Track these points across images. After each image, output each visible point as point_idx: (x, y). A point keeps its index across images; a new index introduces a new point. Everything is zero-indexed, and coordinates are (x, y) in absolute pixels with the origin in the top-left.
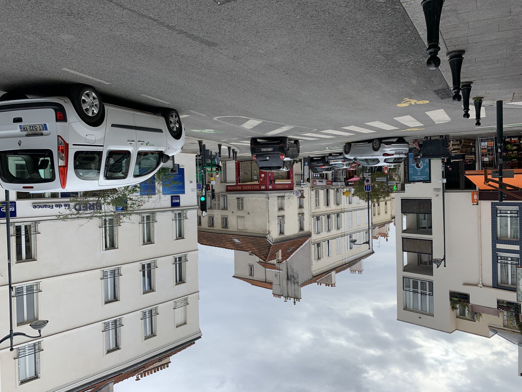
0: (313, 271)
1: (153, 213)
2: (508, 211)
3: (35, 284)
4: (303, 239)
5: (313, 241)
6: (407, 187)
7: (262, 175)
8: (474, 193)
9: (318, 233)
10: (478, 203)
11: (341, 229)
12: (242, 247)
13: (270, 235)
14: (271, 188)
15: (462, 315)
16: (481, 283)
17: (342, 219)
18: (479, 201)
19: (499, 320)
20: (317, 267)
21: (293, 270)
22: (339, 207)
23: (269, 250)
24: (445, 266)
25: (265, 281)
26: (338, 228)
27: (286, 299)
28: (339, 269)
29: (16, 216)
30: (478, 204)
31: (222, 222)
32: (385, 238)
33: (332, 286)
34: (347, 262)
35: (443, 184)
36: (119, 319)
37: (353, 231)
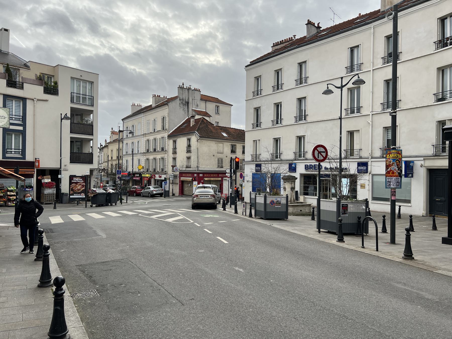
0: (167, 108)
2: (14, 153)
3: (349, 115)
4: (174, 134)
5: (167, 132)
6: (88, 173)
8: (38, 167)
9: (163, 138)
10: (35, 159)
11: (146, 140)
12: (221, 129)
13: (197, 138)
14: (195, 175)
15: (50, 77)
16: (35, 102)
17: (145, 148)
18: (34, 161)
20: (164, 112)
21: (183, 109)
22: (147, 157)
23: (199, 127)
24: (61, 114)
25: (207, 102)
26: (148, 140)
27: (190, 87)
28: (149, 109)
29: (358, 163)
30: (35, 158)
31: (236, 149)
32: (114, 130)
33: (155, 95)
34: (143, 114)
35: (61, 174)
36: (298, 85)
37: (137, 138)
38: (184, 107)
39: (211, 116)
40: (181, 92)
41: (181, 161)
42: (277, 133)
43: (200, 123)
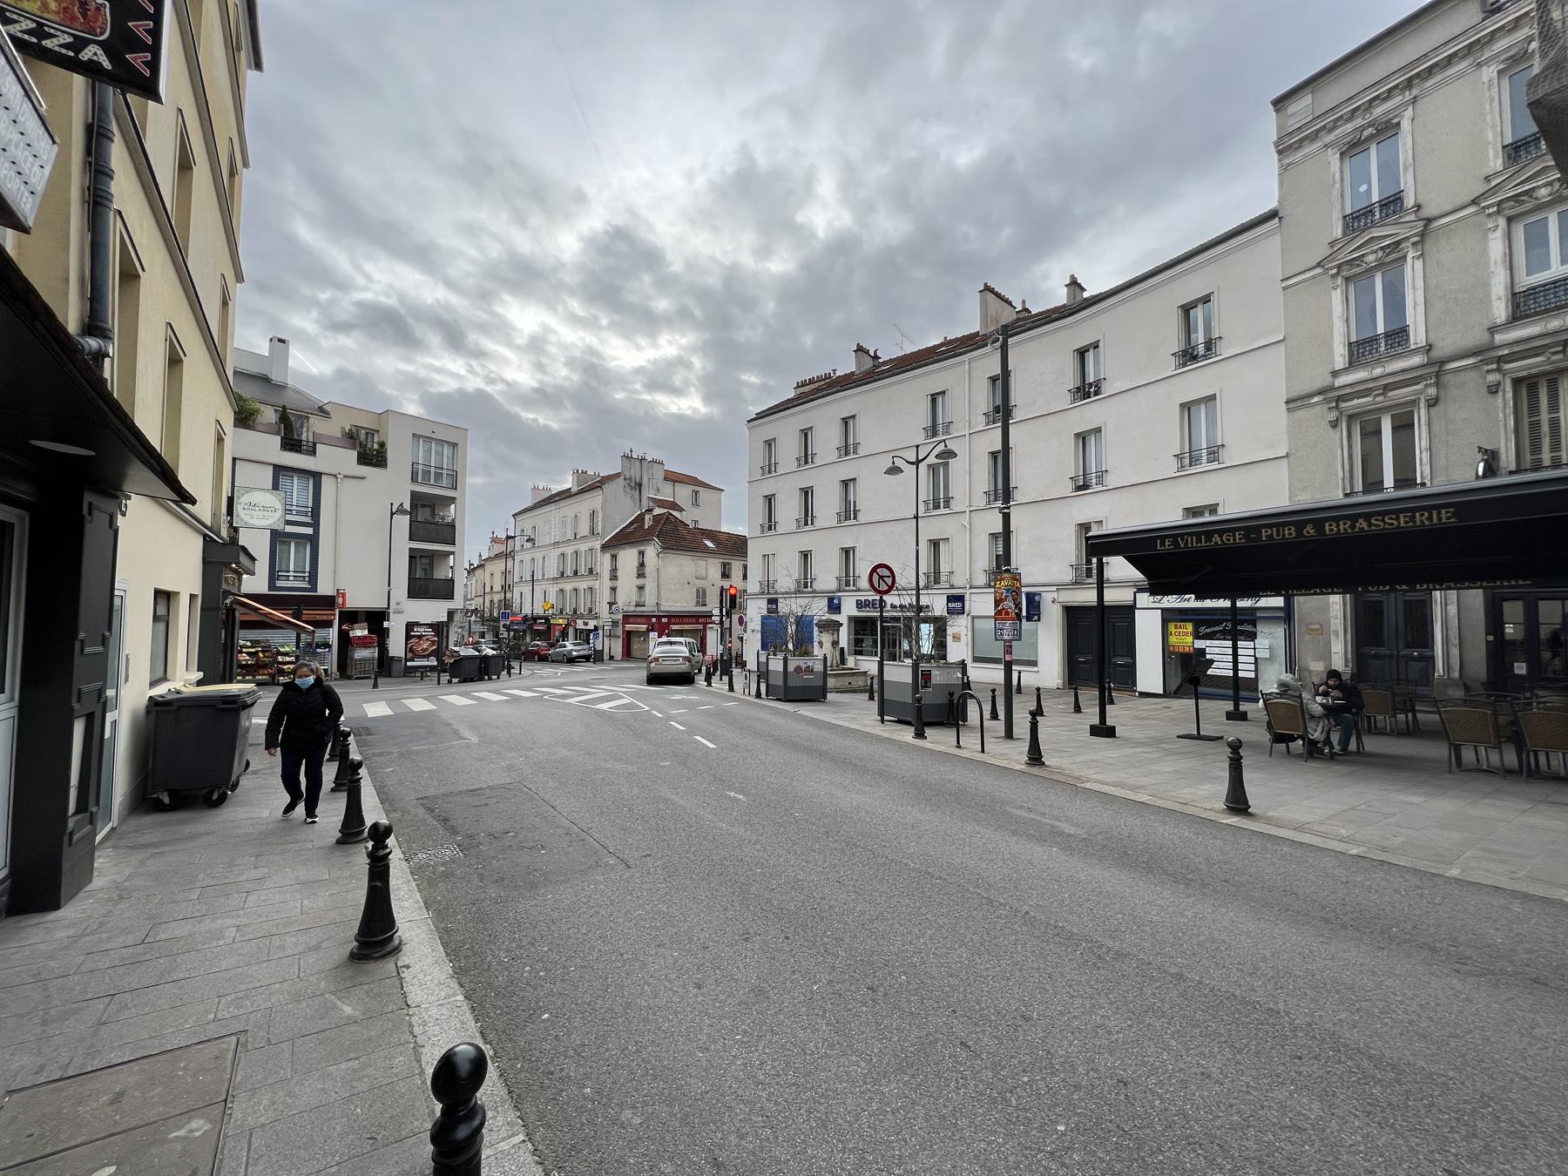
1: (798, 591)
15: (371, 433)
16: (339, 480)
19: (317, 425)
20: (595, 501)
22: (561, 586)
24: (392, 504)
28: (565, 495)
35: (388, 620)
40: (628, 465)
42: (806, 541)
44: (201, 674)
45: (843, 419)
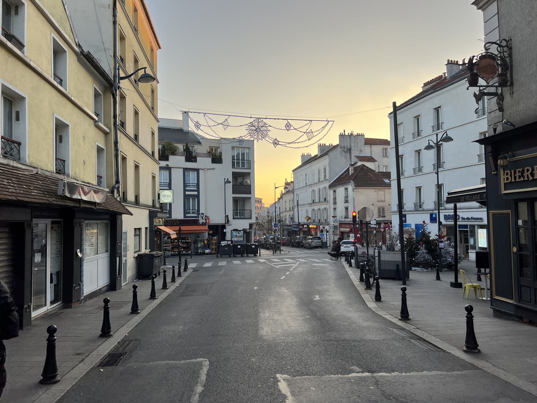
0: (327, 158)
6: (248, 226)
7: (254, 247)
12: (384, 175)
13: (353, 188)
17: (311, 198)
20: (325, 162)
21: (345, 157)
24: (225, 179)
27: (352, 133)
28: (316, 158)
33: (320, 144)
34: (308, 164)
38: (346, 155)
39: (376, 161)
40: (343, 140)
41: (340, 211)
42: (419, 181)
43: (358, 171)
44: (150, 250)
45: (435, 109)
